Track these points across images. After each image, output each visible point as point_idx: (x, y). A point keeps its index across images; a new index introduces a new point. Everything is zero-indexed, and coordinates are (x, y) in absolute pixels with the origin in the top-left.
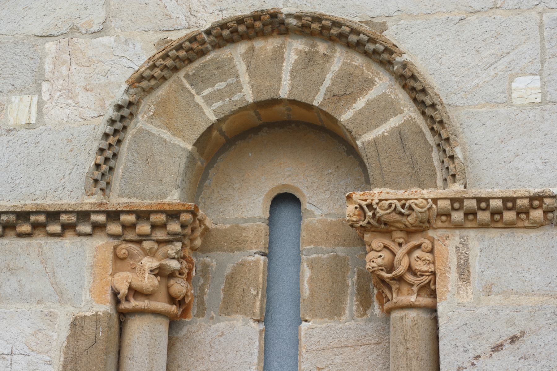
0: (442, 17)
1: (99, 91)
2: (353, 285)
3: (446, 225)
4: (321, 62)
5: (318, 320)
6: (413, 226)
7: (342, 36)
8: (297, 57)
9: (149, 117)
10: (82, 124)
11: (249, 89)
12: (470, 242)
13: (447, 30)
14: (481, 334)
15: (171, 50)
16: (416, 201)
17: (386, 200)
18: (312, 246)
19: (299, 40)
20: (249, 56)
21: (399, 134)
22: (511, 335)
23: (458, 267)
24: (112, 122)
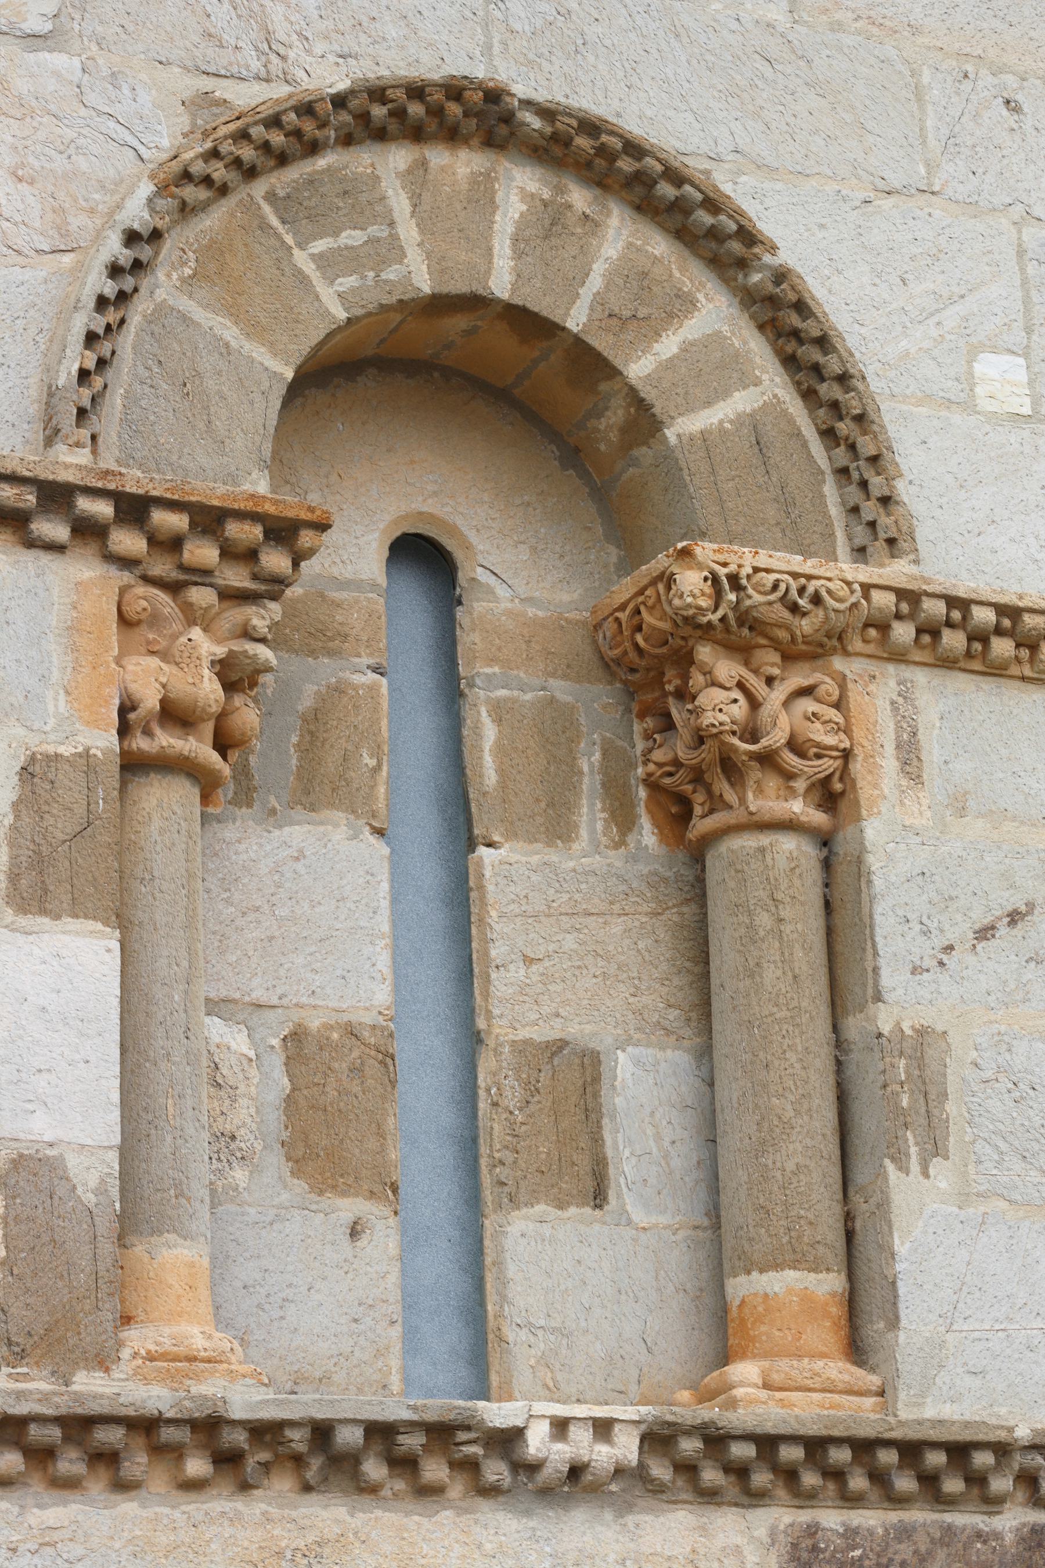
0: (826, 188)
1: (50, 188)
2: (592, 772)
3: (870, 649)
4: (579, 230)
5: (520, 845)
6: (803, 642)
7: (642, 180)
8: (524, 208)
9: (183, 280)
10: (11, 262)
11: (419, 259)
12: (918, 695)
13: (838, 218)
14: (951, 898)
15: (256, 123)
16: (829, 584)
17: (767, 571)
18: (496, 669)
19: (528, 169)
20: (417, 177)
21: (754, 429)
22: (1010, 908)
23: (898, 747)
24: (115, 271)
